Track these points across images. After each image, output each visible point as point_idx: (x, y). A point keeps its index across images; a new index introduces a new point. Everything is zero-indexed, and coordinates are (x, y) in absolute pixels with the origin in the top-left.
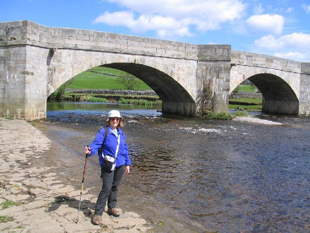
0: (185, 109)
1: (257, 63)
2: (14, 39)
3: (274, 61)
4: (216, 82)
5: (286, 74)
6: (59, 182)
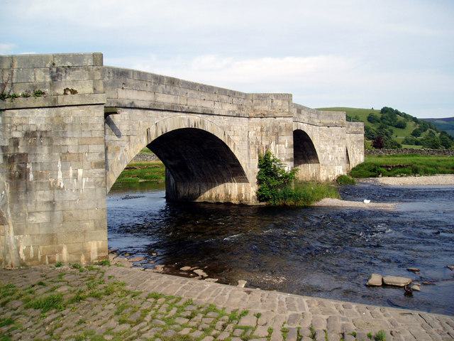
0: (227, 194)
2: (74, 92)
4: (275, 149)
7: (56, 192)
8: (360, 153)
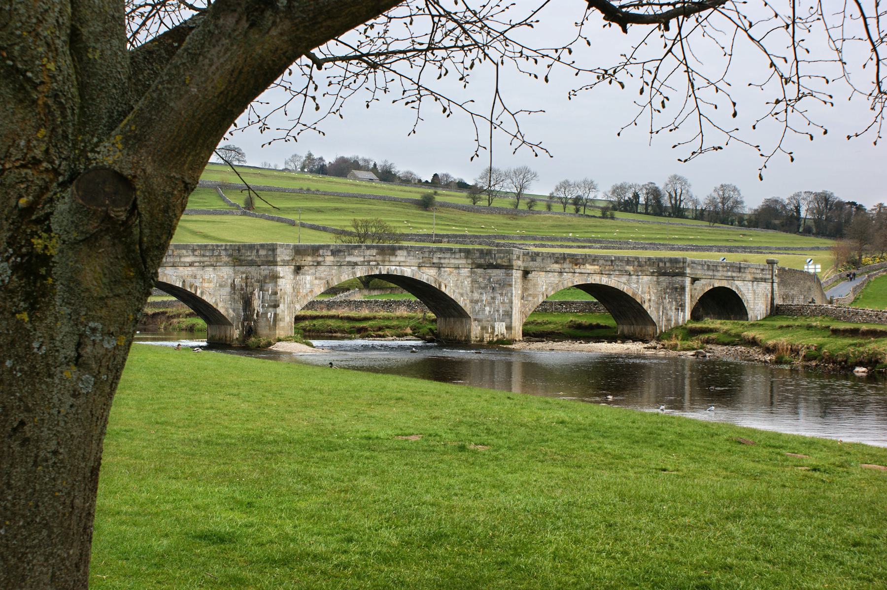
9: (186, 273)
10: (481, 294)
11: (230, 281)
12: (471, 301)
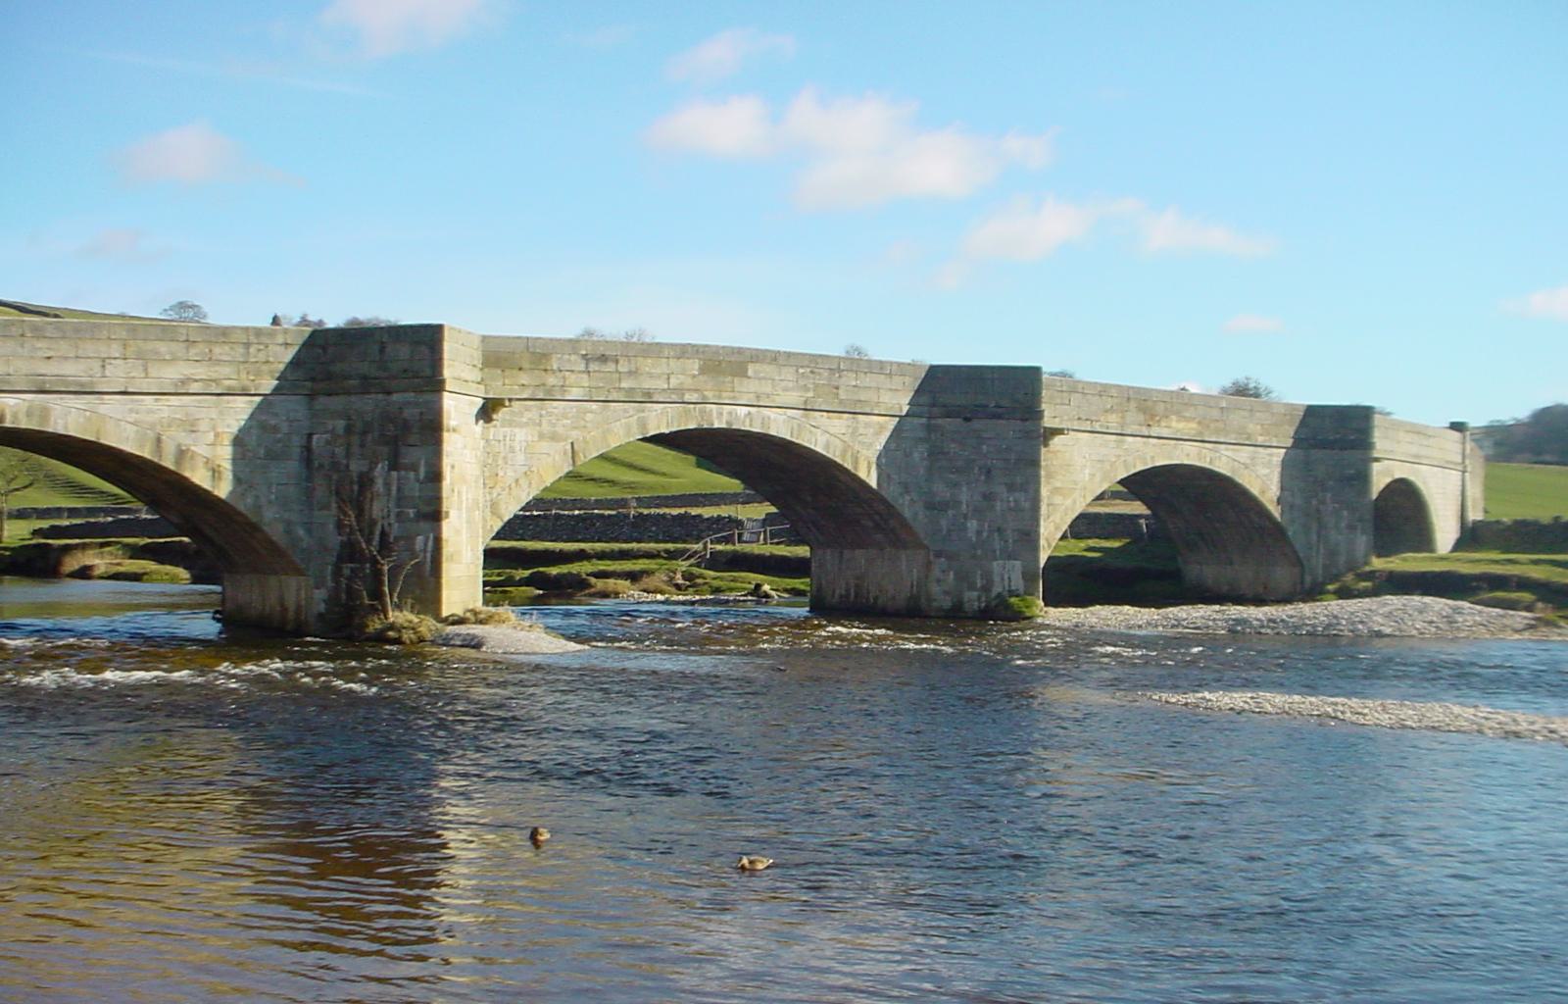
0: (282, 605)
1: (647, 384)
3: (751, 370)
4: (387, 485)
5: (839, 424)
6: (336, 915)
7: (386, 498)
8: (1351, 528)
9: (166, 413)
10: (956, 485)
11: (297, 441)
12: (930, 506)
